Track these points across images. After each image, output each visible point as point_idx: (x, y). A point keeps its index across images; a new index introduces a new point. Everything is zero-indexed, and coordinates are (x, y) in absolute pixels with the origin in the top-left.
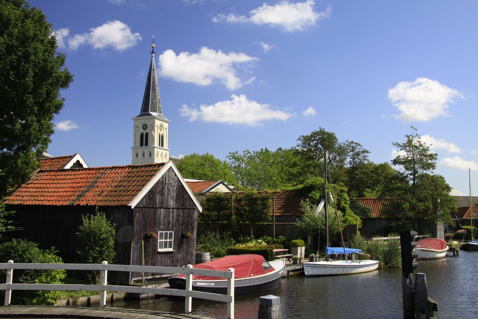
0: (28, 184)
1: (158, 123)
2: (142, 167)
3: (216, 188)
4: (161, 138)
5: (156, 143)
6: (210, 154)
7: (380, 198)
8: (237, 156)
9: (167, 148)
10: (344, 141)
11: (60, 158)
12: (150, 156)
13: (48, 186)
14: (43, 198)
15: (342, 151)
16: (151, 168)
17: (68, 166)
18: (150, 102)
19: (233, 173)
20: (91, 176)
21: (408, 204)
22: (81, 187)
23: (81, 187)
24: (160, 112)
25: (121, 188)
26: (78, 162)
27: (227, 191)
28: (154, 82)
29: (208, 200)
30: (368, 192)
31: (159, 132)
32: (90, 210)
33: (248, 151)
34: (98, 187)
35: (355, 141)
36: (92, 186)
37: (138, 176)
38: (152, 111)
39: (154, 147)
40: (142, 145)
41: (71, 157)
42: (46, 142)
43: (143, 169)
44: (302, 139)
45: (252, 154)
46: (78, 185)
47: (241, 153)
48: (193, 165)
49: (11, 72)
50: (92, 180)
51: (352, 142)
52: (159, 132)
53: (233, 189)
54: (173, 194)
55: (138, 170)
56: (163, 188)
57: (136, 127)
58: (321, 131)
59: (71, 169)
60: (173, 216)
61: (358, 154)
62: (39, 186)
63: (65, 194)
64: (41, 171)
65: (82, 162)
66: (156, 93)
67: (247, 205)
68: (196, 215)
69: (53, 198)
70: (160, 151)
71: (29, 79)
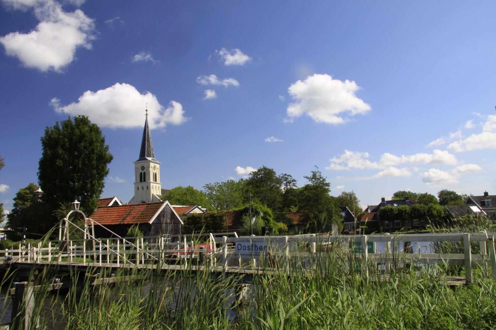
0: (94, 214)
1: (152, 165)
2: (153, 204)
3: (193, 211)
4: (155, 176)
5: (152, 180)
6: (191, 186)
7: (297, 212)
8: (210, 186)
9: (159, 183)
10: (280, 174)
11: (106, 199)
12: (148, 189)
13: (105, 215)
14: (104, 221)
15: (279, 181)
16: (158, 205)
17: (110, 205)
18: (146, 153)
19: (207, 198)
20: (127, 209)
21: (312, 215)
22: (123, 215)
23: (123, 215)
24: (154, 157)
25: (144, 215)
26: (116, 201)
27: (200, 212)
28: (148, 135)
29: (188, 219)
30: (292, 208)
31: (153, 171)
32: (129, 225)
33: (217, 183)
34: (132, 215)
35: (287, 174)
36: (129, 214)
37: (152, 209)
38: (147, 157)
39: (150, 182)
40: (141, 181)
41: (112, 199)
42: (101, 192)
43: (154, 205)
44: (252, 174)
45: (221, 184)
46: (121, 214)
47: (213, 184)
48: (179, 194)
49: (86, 160)
50: (128, 211)
51: (285, 175)
52: (153, 171)
53: (206, 210)
54: (169, 216)
55: (151, 205)
56: (164, 214)
57: (136, 169)
58: (264, 168)
59: (111, 207)
60: (170, 227)
61: (289, 182)
62: (100, 215)
63: (115, 219)
64: (99, 207)
65: (118, 201)
66: (150, 143)
67: (211, 220)
68: (180, 226)
69: (109, 221)
70: (155, 185)
71: (94, 162)
